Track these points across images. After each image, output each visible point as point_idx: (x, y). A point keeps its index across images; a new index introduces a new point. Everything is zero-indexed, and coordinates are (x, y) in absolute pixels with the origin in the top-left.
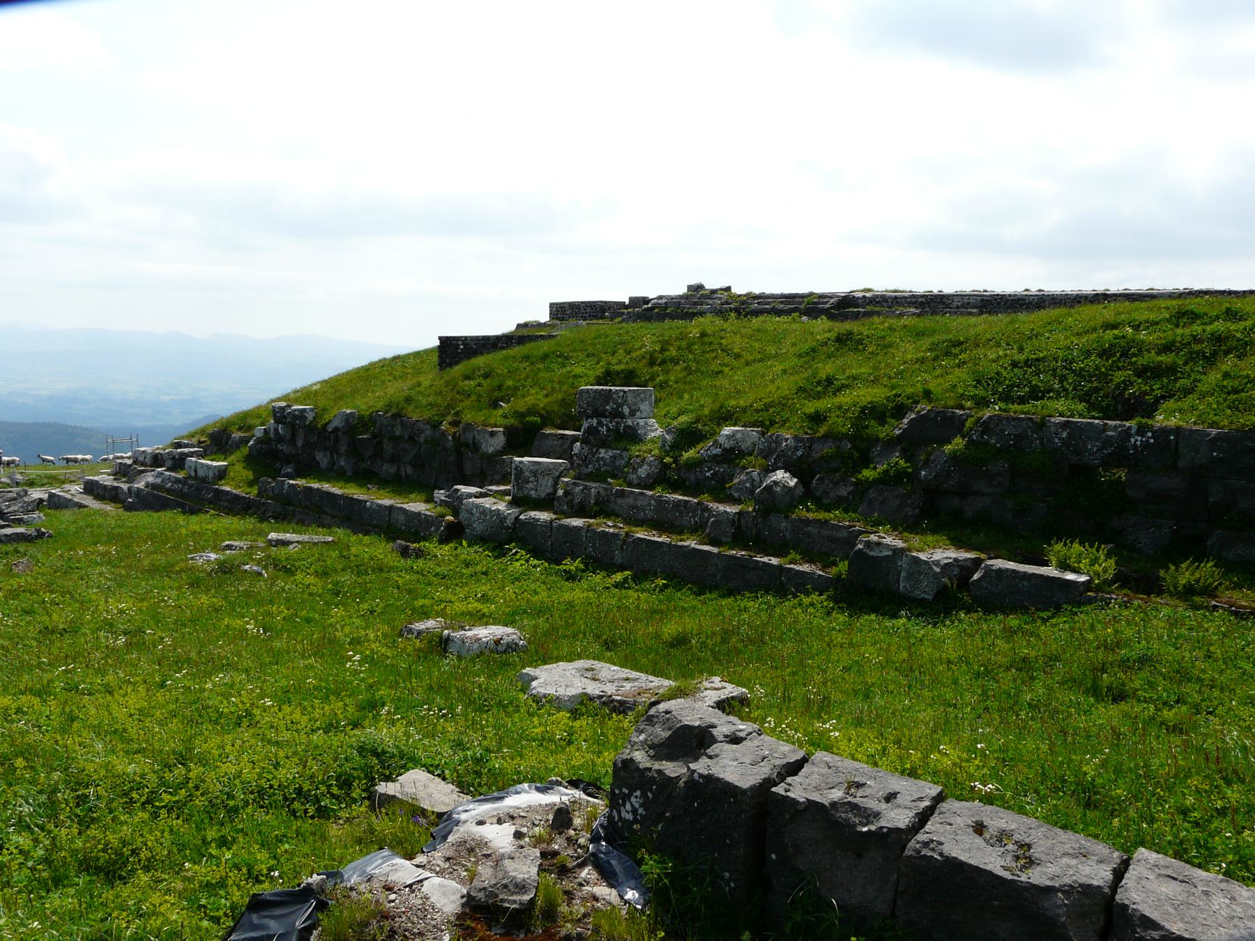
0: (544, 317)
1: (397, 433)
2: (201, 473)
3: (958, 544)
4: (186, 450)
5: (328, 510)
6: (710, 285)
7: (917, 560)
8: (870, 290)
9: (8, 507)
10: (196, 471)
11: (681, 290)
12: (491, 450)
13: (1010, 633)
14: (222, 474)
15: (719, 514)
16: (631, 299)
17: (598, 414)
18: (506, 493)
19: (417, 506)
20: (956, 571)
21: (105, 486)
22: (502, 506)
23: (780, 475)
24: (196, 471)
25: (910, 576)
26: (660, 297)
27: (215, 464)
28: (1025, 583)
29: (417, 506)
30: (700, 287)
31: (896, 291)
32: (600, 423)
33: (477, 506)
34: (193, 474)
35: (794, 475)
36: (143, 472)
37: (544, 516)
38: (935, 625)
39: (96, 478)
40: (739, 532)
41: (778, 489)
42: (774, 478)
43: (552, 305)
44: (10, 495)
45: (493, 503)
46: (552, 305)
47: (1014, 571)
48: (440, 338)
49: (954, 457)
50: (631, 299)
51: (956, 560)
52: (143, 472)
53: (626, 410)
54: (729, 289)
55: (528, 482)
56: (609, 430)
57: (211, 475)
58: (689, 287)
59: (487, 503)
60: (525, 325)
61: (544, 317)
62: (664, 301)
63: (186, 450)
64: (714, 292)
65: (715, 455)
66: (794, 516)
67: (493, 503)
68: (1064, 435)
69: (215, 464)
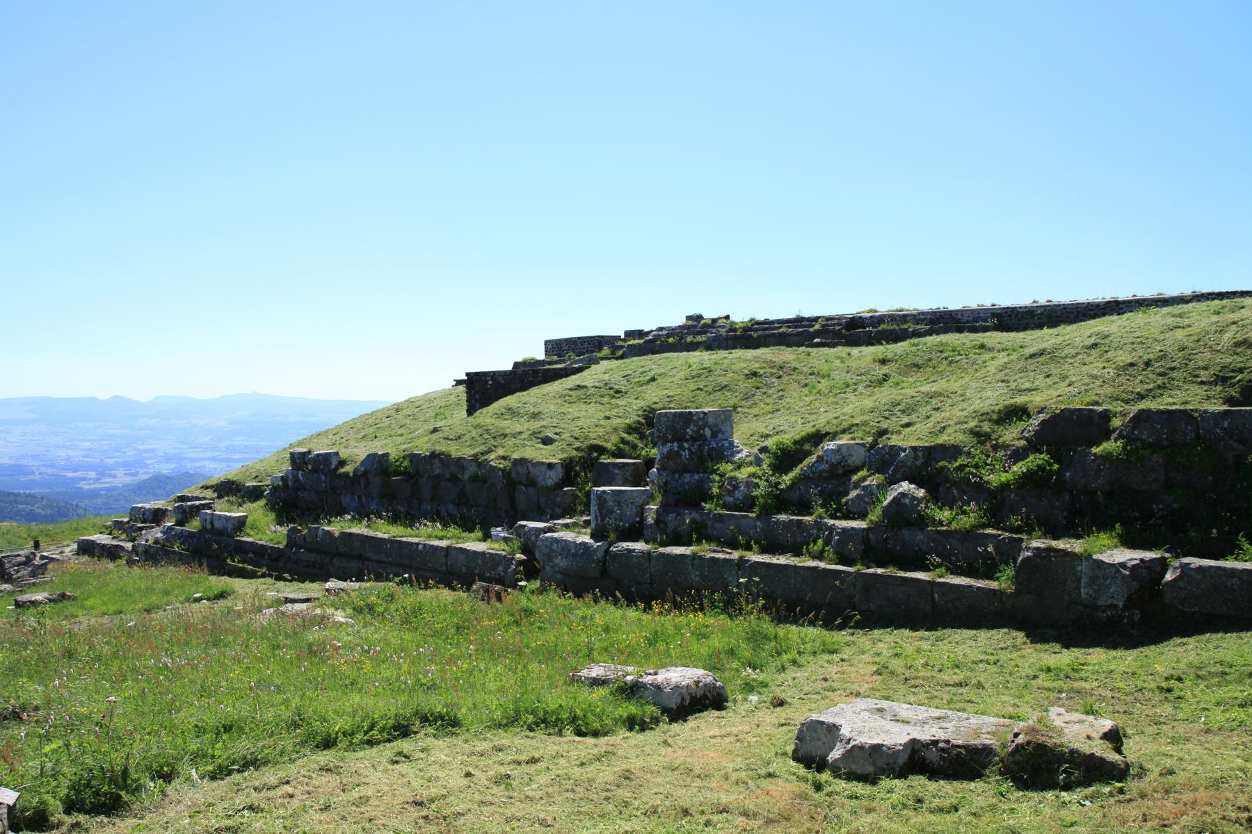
0: (541, 356)
1: (437, 471)
2: (218, 525)
3: (1129, 542)
4: (197, 503)
5: (370, 555)
6: (709, 314)
7: (1100, 564)
9: (18, 572)
10: (212, 523)
12: (550, 482)
13: (364, 610)
15: (844, 529)
18: (587, 523)
19: (474, 544)
21: (104, 545)
22: (586, 538)
23: (905, 486)
24: (212, 523)
25: (1092, 581)
26: (661, 329)
27: (234, 515)
28: (1234, 581)
29: (474, 544)
30: (700, 317)
31: (871, 311)
33: (556, 540)
34: (209, 527)
35: (920, 485)
36: (141, 529)
37: (639, 546)
38: (731, 617)
39: (90, 538)
40: (871, 548)
41: (907, 501)
42: (901, 490)
43: (547, 343)
44: (19, 559)
45: (574, 534)
46: (547, 343)
47: (816, 568)
48: (467, 374)
49: (1107, 457)
51: (1142, 560)
52: (141, 529)
53: (708, 433)
54: (727, 317)
56: (691, 453)
58: (689, 318)
59: (568, 536)
60: (524, 363)
62: (664, 332)
63: (197, 503)
64: (714, 321)
65: (821, 471)
67: (574, 534)
68: (1226, 424)
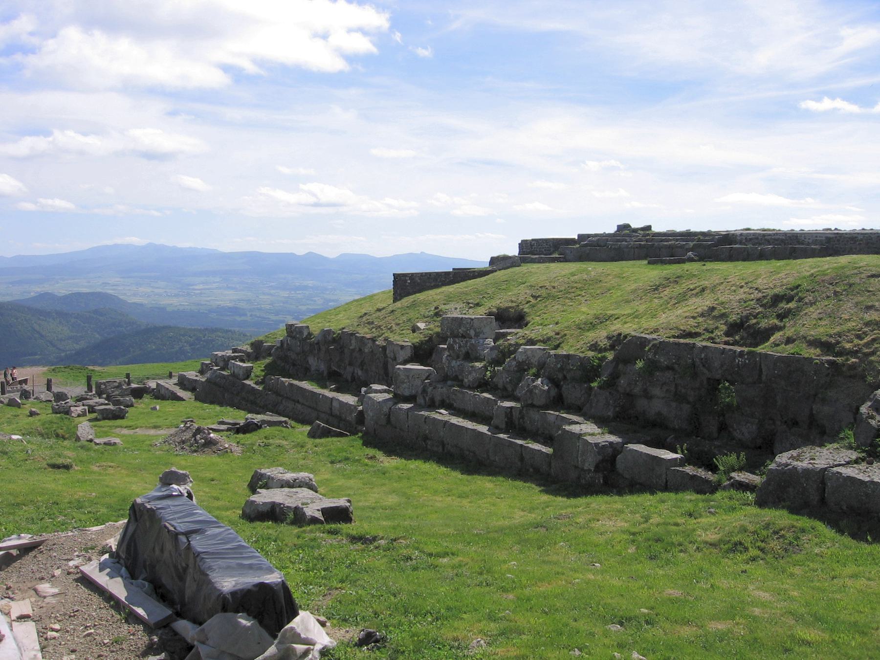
6: (635, 225)
8: (749, 229)
11: (611, 229)
14: (248, 374)
16: (579, 236)
17: (455, 336)
20: (610, 450)
27: (245, 365)
30: (627, 226)
32: (454, 342)
41: (537, 391)
43: (396, 276)
46: (396, 276)
50: (579, 236)
51: (611, 443)
53: (472, 333)
55: (403, 383)
57: (241, 373)
61: (514, 251)
66: (772, 466)
69: (245, 365)
